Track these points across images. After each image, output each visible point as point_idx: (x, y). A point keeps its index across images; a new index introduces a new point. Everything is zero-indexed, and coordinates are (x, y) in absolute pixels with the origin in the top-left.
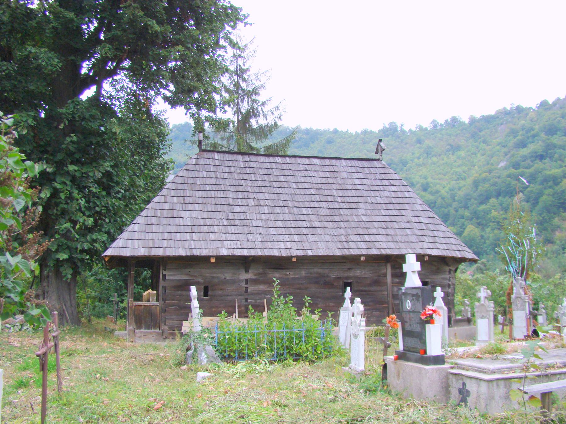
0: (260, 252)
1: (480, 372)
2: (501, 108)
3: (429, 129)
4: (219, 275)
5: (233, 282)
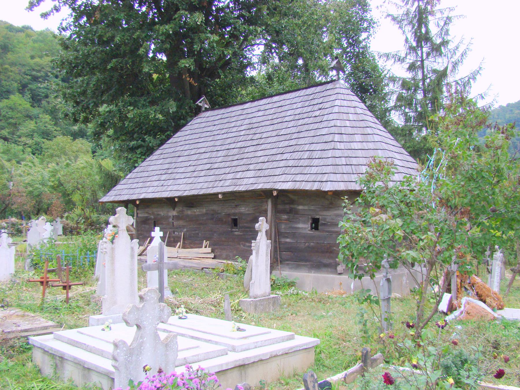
1: (27, 331)
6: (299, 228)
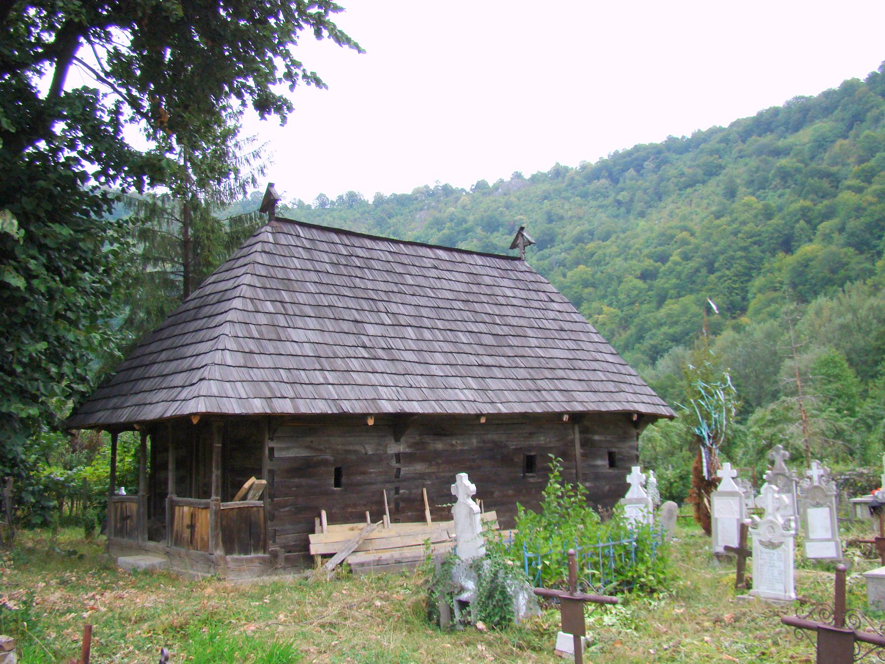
0: (235, 406)
2: (422, 185)
3: (313, 208)
4: (357, 447)
5: (379, 459)
6: (598, 466)
